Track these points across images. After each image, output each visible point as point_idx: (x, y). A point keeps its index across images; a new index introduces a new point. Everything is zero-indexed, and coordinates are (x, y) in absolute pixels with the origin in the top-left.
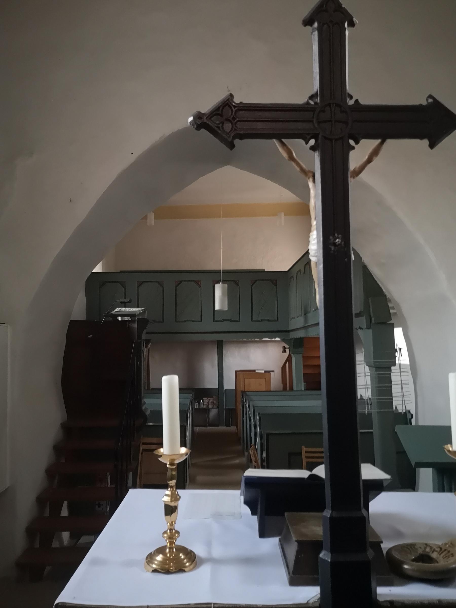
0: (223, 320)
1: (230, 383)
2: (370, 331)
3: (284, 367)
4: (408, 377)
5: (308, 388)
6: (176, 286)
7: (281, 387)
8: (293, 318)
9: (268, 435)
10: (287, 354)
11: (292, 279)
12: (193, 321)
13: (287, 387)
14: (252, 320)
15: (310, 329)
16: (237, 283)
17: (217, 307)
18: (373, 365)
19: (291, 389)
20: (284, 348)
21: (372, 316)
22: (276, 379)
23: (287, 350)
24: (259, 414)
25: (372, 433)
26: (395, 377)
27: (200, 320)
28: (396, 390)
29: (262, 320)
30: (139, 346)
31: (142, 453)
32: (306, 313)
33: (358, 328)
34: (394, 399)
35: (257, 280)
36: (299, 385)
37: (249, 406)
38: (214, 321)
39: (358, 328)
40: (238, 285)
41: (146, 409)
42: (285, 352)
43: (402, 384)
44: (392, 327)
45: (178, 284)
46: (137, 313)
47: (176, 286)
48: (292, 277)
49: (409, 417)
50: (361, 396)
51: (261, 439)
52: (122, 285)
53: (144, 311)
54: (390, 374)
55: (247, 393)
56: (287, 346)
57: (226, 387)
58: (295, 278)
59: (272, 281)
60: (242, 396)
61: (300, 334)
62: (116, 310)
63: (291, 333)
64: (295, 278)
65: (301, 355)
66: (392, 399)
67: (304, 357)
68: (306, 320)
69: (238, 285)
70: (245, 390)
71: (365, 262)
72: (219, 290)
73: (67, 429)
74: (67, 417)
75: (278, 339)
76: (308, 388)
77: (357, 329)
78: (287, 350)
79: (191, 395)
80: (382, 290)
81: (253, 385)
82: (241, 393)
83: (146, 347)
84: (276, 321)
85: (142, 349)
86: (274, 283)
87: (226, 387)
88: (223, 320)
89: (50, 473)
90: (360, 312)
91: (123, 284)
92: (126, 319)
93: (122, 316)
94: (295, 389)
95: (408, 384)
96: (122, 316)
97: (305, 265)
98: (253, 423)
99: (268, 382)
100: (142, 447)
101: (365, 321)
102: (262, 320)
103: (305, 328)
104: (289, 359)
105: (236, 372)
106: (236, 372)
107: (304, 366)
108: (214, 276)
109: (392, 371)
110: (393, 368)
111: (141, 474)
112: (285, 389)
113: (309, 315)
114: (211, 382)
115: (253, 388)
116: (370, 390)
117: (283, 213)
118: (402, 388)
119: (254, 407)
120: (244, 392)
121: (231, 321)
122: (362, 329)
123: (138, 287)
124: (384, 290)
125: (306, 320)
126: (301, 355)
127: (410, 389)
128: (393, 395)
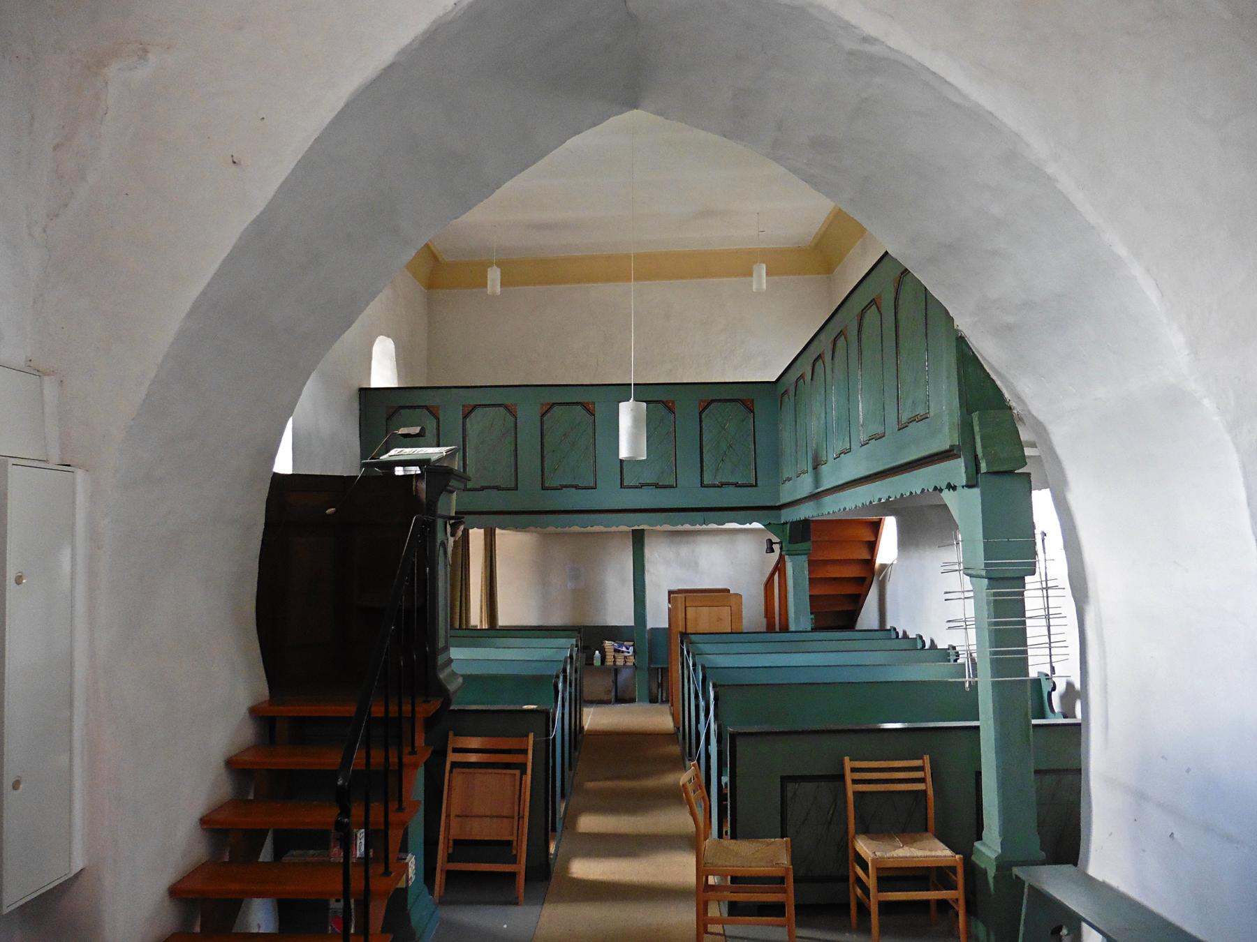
0: (642, 486)
1: (658, 617)
2: (976, 492)
3: (769, 584)
4: (1064, 603)
5: (820, 626)
6: (543, 415)
7: (761, 623)
8: (789, 479)
9: (733, 736)
10: (775, 556)
11: (786, 397)
12: (576, 487)
13: (775, 624)
14: (702, 485)
15: (827, 500)
16: (669, 407)
17: (624, 453)
18: (983, 573)
19: (785, 628)
20: (770, 543)
21: (980, 455)
22: (752, 612)
23: (776, 547)
24: (714, 686)
25: (978, 728)
26: (1033, 602)
27: (592, 485)
28: (1035, 631)
29: (722, 485)
30: (427, 531)
31: (451, 772)
32: (816, 466)
33: (944, 486)
34: (1030, 652)
35: (713, 401)
36: (799, 617)
37: (694, 665)
38: (622, 486)
39: (944, 486)
40: (671, 410)
41: (454, 674)
42: (773, 551)
43: (1048, 617)
44: (1026, 484)
45: (547, 411)
46: (434, 458)
47: (543, 415)
48: (786, 392)
49: (1046, 687)
50: (932, 641)
51: (719, 741)
52: (430, 412)
53: (451, 455)
54: (1022, 594)
55: (693, 637)
56: (775, 539)
57: (650, 624)
58: (792, 392)
59: (743, 402)
60: (682, 643)
61: (806, 512)
62: (393, 452)
63: (784, 512)
64: (792, 392)
65: (804, 558)
66: (1025, 652)
67: (811, 563)
68: (817, 481)
69: (671, 410)
70: (689, 631)
71: (960, 328)
72: (627, 414)
73: (264, 719)
74: (267, 691)
75: (756, 525)
76: (820, 626)
77: (941, 490)
78: (776, 547)
79: (574, 641)
80: (1002, 395)
81: (702, 618)
82: (681, 636)
83: (453, 535)
84: (751, 486)
85: (440, 536)
86: (749, 406)
87: (650, 624)
88: (642, 486)
89: (213, 825)
90: (952, 448)
91: (433, 412)
92: (415, 470)
93: (404, 463)
94: (792, 627)
95: (1059, 616)
96: (404, 463)
97: (816, 360)
98: (702, 704)
99: (737, 615)
100: (452, 757)
101: (963, 469)
102: (722, 485)
103: (815, 497)
104: (779, 567)
105: (670, 593)
106: (670, 593)
107: (812, 581)
108: (621, 391)
109: (1027, 586)
110: (1028, 579)
111: (448, 816)
112: (770, 628)
113: (824, 469)
114: (619, 613)
115: (703, 628)
116: (972, 633)
117: (763, 268)
118: (1049, 627)
119: (703, 668)
120: (684, 635)
121: (657, 486)
122: (954, 488)
123: (465, 417)
124: (1007, 395)
125: (817, 481)
126: (804, 558)
127: (1067, 631)
128: (1029, 642)
